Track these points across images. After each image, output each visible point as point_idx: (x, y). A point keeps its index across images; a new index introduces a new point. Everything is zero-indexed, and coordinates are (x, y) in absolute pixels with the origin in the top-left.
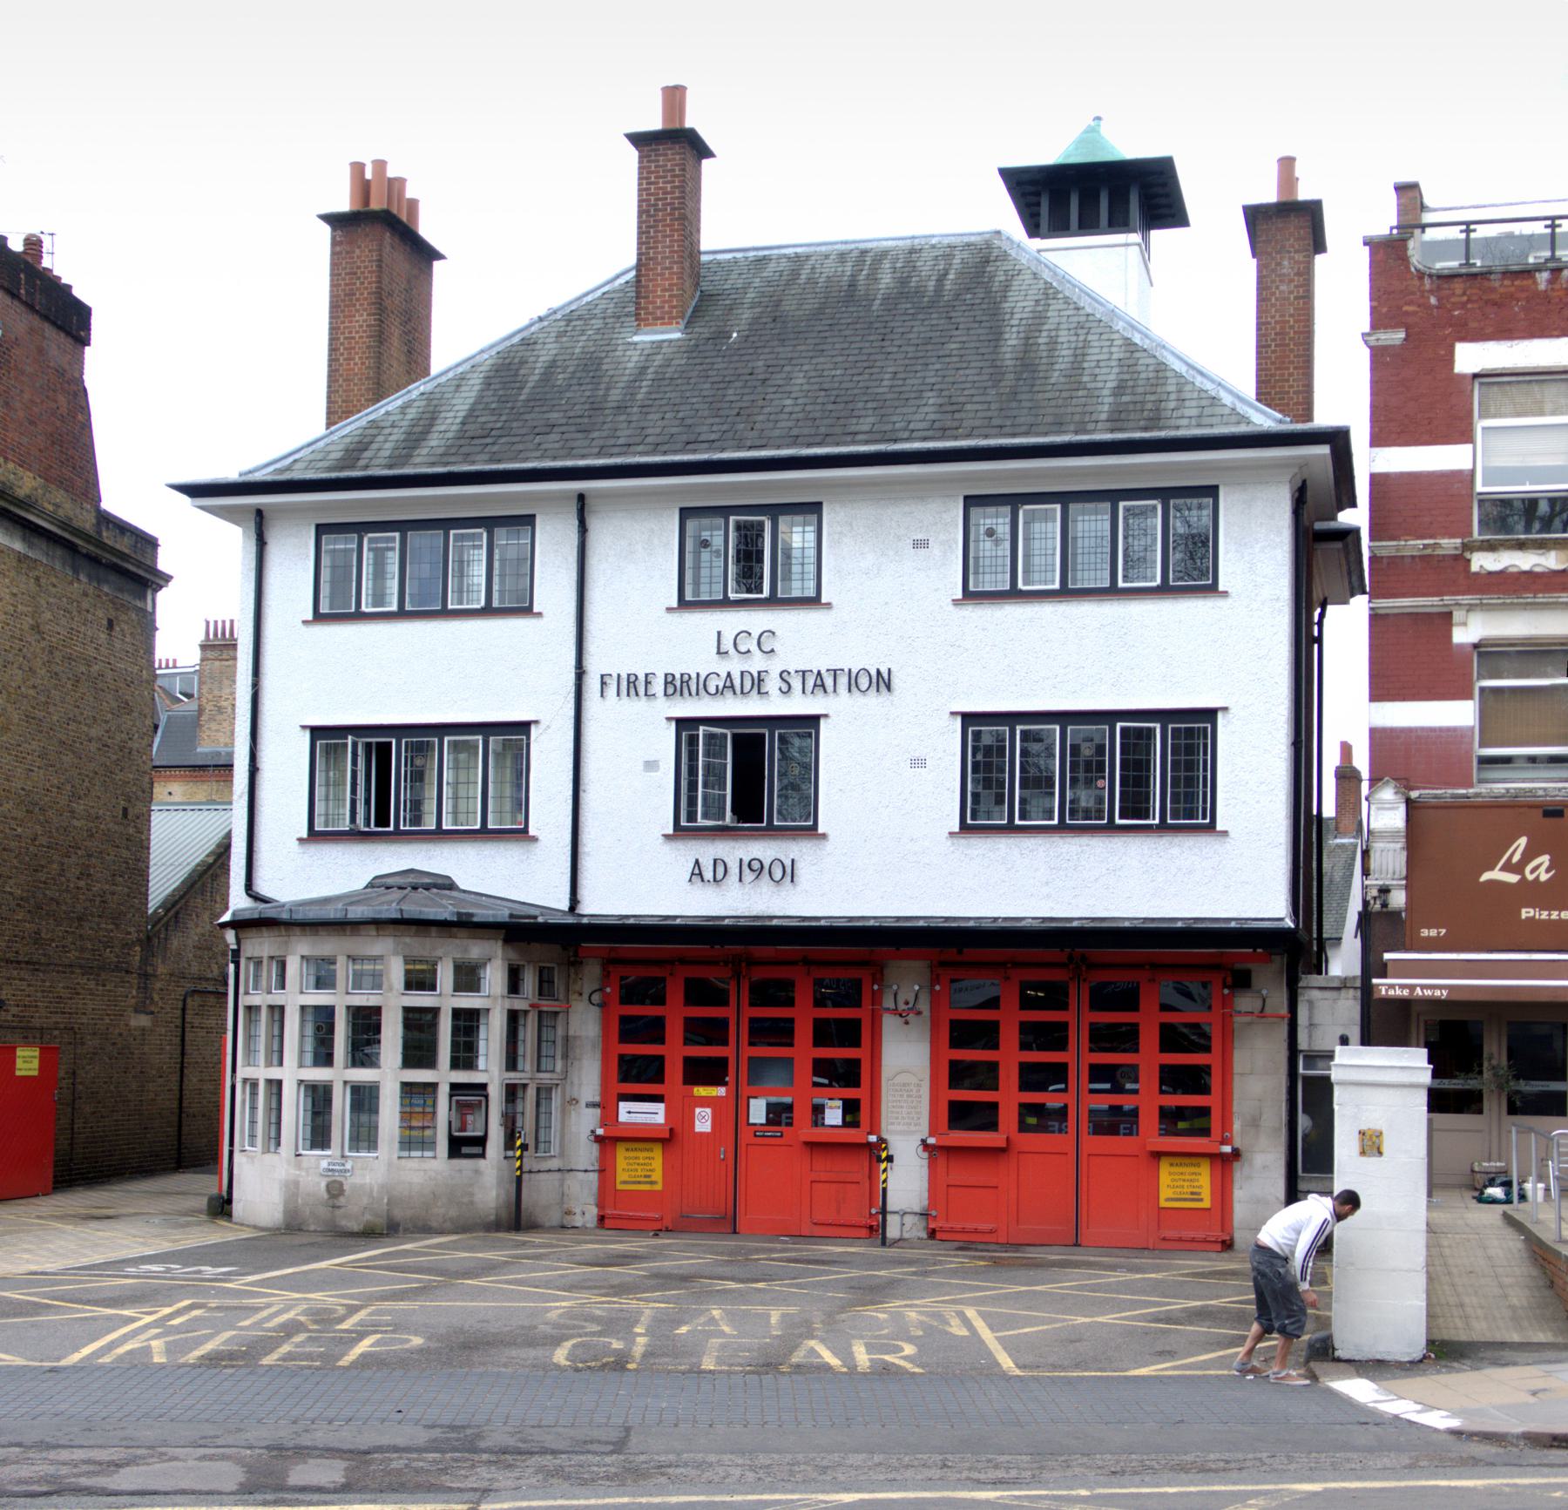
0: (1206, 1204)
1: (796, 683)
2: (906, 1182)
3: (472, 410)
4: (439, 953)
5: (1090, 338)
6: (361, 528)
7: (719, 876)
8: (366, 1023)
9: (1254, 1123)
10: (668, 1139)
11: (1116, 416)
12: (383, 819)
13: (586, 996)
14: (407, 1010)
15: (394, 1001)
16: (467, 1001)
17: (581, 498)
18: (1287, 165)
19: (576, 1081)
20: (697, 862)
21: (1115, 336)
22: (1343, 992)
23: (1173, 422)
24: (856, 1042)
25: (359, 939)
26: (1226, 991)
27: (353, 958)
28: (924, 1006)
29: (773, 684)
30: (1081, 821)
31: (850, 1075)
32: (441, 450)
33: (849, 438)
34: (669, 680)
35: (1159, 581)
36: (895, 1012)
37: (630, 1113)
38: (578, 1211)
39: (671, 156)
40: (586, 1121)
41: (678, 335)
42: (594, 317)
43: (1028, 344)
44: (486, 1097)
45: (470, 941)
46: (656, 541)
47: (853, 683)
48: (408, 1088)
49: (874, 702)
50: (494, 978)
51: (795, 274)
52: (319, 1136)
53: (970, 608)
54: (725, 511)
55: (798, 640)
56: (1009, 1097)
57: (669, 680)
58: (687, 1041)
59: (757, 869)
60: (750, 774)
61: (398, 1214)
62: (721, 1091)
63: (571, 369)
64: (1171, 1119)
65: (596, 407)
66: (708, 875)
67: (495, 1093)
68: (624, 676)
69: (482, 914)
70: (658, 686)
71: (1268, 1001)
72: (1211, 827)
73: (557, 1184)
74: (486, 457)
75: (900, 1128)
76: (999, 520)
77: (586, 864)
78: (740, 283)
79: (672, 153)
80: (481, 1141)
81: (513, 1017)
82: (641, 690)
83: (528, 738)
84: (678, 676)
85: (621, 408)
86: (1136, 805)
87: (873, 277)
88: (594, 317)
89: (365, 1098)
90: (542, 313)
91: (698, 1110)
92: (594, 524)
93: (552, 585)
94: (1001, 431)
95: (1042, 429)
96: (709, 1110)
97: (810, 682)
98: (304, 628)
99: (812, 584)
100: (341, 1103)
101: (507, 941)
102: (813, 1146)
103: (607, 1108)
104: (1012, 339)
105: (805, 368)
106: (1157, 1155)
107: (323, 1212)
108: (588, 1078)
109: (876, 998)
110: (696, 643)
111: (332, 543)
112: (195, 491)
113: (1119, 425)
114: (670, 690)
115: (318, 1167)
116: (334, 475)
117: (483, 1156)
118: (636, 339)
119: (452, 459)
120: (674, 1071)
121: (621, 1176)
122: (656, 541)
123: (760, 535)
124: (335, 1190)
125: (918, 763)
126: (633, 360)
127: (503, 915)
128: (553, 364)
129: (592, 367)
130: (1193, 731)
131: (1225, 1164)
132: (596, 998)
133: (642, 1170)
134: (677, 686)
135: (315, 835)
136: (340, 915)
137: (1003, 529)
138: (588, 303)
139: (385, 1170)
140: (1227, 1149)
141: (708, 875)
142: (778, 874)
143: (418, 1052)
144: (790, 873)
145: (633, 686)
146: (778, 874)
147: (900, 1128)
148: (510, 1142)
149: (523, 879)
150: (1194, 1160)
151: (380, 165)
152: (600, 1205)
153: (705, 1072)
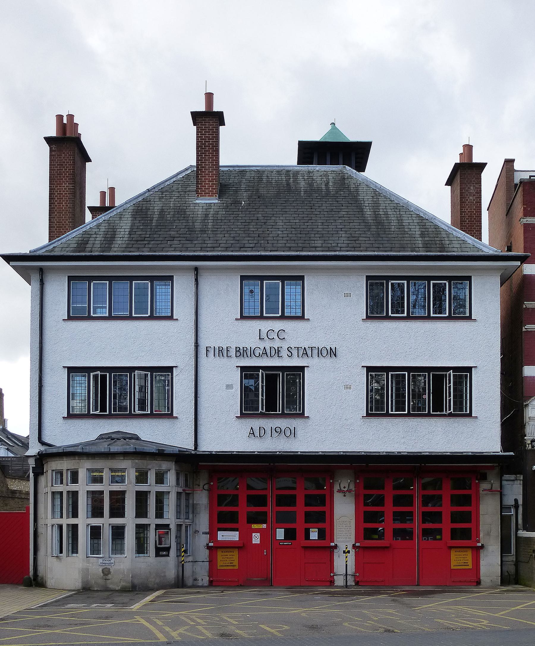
0: (470, 567)
1: (295, 352)
2: (344, 563)
3: (131, 229)
4: (149, 467)
5: (401, 213)
6: (90, 279)
7: (262, 434)
8: (117, 499)
9: (488, 534)
10: (242, 546)
11: (425, 246)
12: (103, 409)
13: (201, 486)
14: (137, 492)
15: (130, 488)
16: (161, 488)
17: (196, 269)
18: (209, 97)
19: (197, 522)
20: (252, 428)
21: (412, 213)
22: (516, 482)
23: (449, 249)
24: (470, 504)
25: (114, 461)
26: (477, 481)
27: (112, 470)
28: (352, 487)
29: (284, 353)
30: (417, 412)
31: (323, 518)
32: (124, 246)
33: (314, 249)
34: (238, 350)
35: (280, 314)
36: (340, 491)
37: (223, 536)
38: (200, 579)
39: (210, 123)
40: (203, 540)
41: (217, 201)
42: (173, 191)
43: (376, 215)
44: (170, 529)
45: (162, 462)
46: (230, 289)
47: (320, 353)
48: (138, 526)
49: (328, 361)
50: (171, 477)
51: (260, 179)
52: (95, 549)
53: (369, 323)
54: (429, 279)
55: (296, 334)
56: (417, 525)
57: (238, 350)
58: (395, 505)
59: (279, 431)
60: (273, 390)
61: (136, 582)
62: (264, 526)
63: (172, 213)
64: (454, 534)
65: (191, 230)
66: (257, 434)
67: (173, 527)
68: (217, 348)
69: (168, 451)
70: (233, 352)
71: (493, 485)
72: (470, 415)
73: (191, 567)
74: (148, 249)
75: (341, 540)
76: (256, 286)
77: (201, 429)
78: (236, 181)
79: (208, 121)
80: (168, 549)
81: (179, 494)
82: (225, 355)
83: (172, 375)
84: (241, 348)
85: (203, 231)
86: (400, 406)
87: (296, 181)
88: (173, 191)
89: (118, 533)
90: (149, 187)
91: (254, 534)
92: (201, 280)
93: (183, 308)
94: (379, 249)
95: (395, 249)
96: (259, 534)
97: (301, 352)
98: (63, 322)
99: (169, 311)
100: (107, 534)
101: (176, 462)
102: (306, 548)
103: (212, 535)
104: (368, 212)
105: (282, 218)
106: (451, 548)
107: (101, 582)
108: (203, 521)
109: (332, 486)
110: (249, 334)
111: (249, 285)
112: (8, 258)
113: (428, 249)
114: (238, 354)
115: (98, 562)
116: (122, 254)
117: (168, 555)
118: (197, 201)
119: (131, 250)
120: (243, 518)
121: (220, 563)
122: (230, 289)
123: (444, 290)
124: (106, 572)
125: (348, 387)
126: (200, 212)
127: (176, 451)
128: (162, 211)
129: (181, 213)
130: (463, 374)
131: (477, 550)
132: (206, 487)
133: (229, 561)
134: (241, 352)
135: (71, 416)
136: (107, 450)
137: (257, 290)
138: (168, 185)
139: (127, 562)
140: (479, 544)
141: (257, 434)
142: (288, 434)
143: (97, 512)
144: (293, 433)
145: (221, 352)
146: (288, 434)
147: (341, 540)
148: (178, 550)
149: (172, 434)
150: (465, 550)
151: (71, 117)
152: (210, 576)
153: (254, 519)
